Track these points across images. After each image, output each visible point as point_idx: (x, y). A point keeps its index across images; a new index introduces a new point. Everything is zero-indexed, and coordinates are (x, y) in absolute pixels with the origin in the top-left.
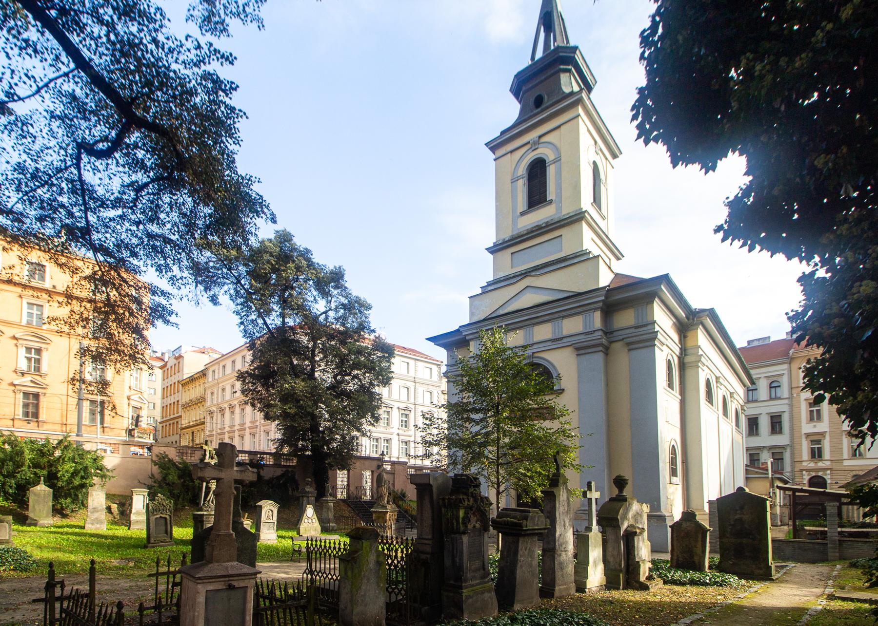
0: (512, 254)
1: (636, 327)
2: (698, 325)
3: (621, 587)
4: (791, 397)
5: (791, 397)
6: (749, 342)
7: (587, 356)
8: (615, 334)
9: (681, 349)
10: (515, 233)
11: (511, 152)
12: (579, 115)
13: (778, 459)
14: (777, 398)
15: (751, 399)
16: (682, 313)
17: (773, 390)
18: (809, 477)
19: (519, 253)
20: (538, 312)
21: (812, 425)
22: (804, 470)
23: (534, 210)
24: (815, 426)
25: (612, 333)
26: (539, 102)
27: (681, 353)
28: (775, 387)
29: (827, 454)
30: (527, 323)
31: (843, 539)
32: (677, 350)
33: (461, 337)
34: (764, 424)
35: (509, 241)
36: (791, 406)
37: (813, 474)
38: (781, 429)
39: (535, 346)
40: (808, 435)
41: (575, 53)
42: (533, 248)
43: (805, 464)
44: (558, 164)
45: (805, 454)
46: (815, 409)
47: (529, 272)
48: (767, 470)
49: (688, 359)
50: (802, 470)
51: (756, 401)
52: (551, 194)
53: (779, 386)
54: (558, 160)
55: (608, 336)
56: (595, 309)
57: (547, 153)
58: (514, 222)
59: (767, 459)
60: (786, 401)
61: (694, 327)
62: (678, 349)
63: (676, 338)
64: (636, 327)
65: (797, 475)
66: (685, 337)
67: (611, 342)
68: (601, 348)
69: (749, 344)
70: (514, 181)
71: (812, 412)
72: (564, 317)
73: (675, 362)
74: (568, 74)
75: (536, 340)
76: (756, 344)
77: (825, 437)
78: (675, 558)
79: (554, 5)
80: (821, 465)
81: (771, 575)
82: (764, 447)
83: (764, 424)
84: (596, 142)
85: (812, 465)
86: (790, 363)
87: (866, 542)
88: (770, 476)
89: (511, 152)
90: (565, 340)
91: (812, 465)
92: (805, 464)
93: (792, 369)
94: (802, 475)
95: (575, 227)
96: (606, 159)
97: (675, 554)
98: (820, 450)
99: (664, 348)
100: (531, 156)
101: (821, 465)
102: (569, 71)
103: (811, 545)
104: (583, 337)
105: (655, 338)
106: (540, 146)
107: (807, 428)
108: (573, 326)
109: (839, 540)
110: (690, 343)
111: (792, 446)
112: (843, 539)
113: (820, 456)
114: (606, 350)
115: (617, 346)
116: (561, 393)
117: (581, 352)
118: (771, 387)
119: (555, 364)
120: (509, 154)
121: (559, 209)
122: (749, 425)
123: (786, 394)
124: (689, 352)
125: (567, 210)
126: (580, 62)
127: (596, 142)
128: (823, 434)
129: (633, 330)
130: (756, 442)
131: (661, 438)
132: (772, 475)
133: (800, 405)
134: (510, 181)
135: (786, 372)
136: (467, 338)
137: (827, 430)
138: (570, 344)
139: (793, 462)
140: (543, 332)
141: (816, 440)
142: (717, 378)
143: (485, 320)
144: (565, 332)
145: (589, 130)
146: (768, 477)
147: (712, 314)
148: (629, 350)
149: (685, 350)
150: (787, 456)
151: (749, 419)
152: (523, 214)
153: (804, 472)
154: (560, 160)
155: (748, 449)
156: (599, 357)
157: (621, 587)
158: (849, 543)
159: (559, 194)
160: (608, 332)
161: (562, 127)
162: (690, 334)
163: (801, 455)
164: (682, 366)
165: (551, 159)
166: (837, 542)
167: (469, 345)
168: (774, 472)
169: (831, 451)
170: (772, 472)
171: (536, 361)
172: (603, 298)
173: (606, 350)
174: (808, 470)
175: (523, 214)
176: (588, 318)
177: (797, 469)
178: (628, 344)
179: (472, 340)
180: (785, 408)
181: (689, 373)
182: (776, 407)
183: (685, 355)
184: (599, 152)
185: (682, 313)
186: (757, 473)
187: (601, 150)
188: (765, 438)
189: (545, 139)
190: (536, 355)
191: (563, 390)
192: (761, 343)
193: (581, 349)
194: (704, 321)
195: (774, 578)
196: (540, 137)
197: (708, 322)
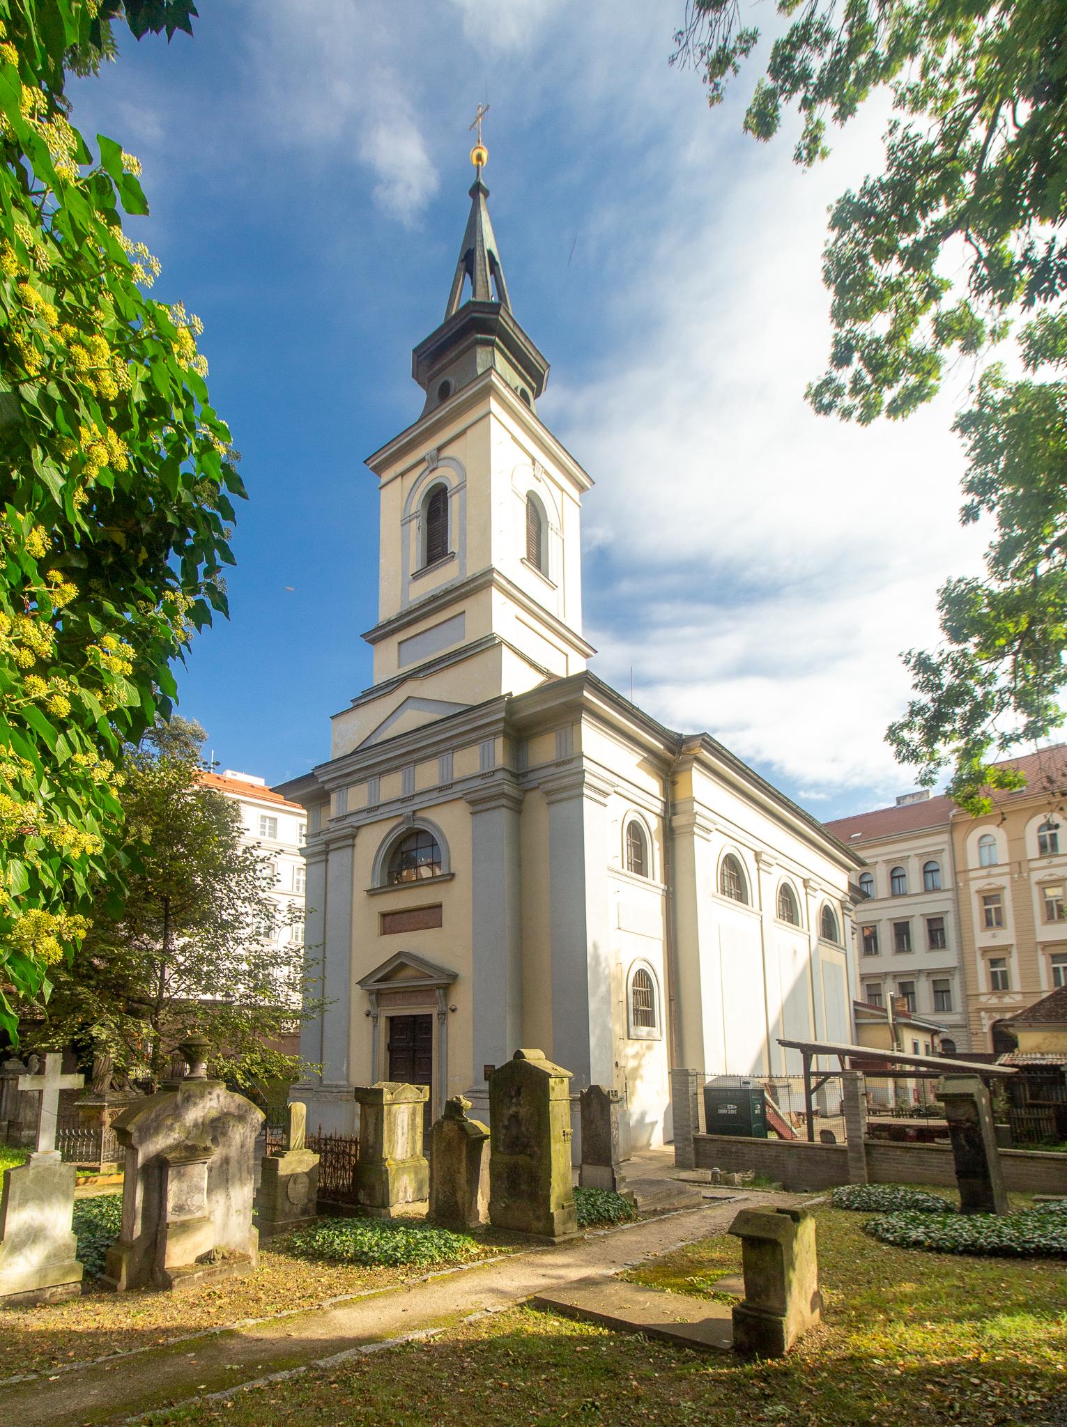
0: (400, 643)
1: (558, 765)
2: (690, 761)
3: (124, 1282)
4: (956, 889)
5: (956, 889)
6: (899, 800)
7: (485, 815)
8: (531, 776)
9: (665, 804)
10: (407, 607)
11: (402, 474)
12: (490, 412)
13: (942, 992)
14: (936, 889)
15: (930, 886)
16: (658, 745)
17: (929, 875)
18: (991, 1022)
19: (410, 641)
20: (417, 741)
21: (989, 933)
22: (983, 1009)
23: (436, 568)
24: (994, 936)
25: (525, 775)
26: (445, 393)
27: (666, 811)
28: (932, 871)
29: (1016, 983)
30: (396, 763)
31: (876, 1141)
32: (658, 807)
33: (315, 787)
34: (919, 933)
35: (397, 620)
36: (957, 902)
37: (998, 1017)
38: (943, 942)
39: (417, 800)
40: (985, 951)
41: (498, 313)
42: (427, 634)
43: (983, 999)
44: (462, 492)
45: (983, 984)
46: (992, 907)
47: (420, 671)
48: (886, 1011)
49: (678, 821)
50: (979, 1010)
51: (905, 895)
52: (453, 546)
53: (938, 870)
54: (462, 487)
55: (522, 780)
56: (495, 735)
57: (446, 474)
58: (405, 592)
59: (890, 991)
60: (949, 895)
61: (687, 766)
62: (659, 804)
63: (654, 786)
64: (558, 765)
65: (973, 1017)
66: (674, 783)
67: (527, 791)
68: (504, 802)
69: (899, 803)
70: (405, 522)
71: (988, 911)
72: (455, 749)
73: (653, 824)
74: (490, 349)
75: (418, 788)
76: (909, 801)
77: (1010, 953)
78: (434, 1196)
79: (479, 238)
80: (1007, 1000)
81: (552, 1233)
82: (886, 974)
83: (886, 937)
84: (534, 460)
85: (994, 1001)
86: (951, 833)
87: (907, 1149)
88: (891, 1021)
89: (402, 474)
90: (456, 788)
91: (994, 1001)
92: (983, 999)
93: (955, 842)
94: (980, 1019)
95: (481, 596)
96: (562, 490)
97: (435, 1187)
98: (1004, 974)
99: (613, 800)
100: (429, 481)
101: (1007, 1000)
102: (491, 343)
103: (824, 1153)
104: (478, 782)
105: (581, 783)
106: (441, 463)
107: (984, 939)
108: (467, 762)
109: (866, 1145)
110: (681, 794)
111: (962, 968)
112: (876, 1141)
113: (1006, 986)
114: (518, 807)
115: (535, 798)
116: (451, 880)
117: (479, 808)
118: (925, 872)
119: (439, 824)
120: (399, 479)
121: (463, 567)
122: (896, 935)
123: (948, 883)
124: (680, 808)
125: (472, 570)
126: (510, 327)
127: (534, 460)
128: (1006, 948)
129: (553, 770)
130: (877, 965)
131: (597, 958)
132: (894, 1020)
133: (969, 897)
134: (399, 523)
135: (946, 846)
136: (327, 787)
137: (1013, 941)
138: (459, 795)
139: (966, 997)
140: (428, 775)
141: (996, 960)
142: (757, 855)
143: (354, 753)
144: (457, 775)
145: (514, 438)
146: (887, 1024)
147: (707, 741)
148: (549, 804)
149: (674, 806)
150: (955, 986)
151: (895, 924)
152: (417, 576)
153: (983, 1014)
154: (465, 486)
155: (863, 978)
156: (501, 819)
157: (124, 1282)
158: (882, 1150)
159: (463, 544)
160: (520, 774)
161: (469, 432)
162: (681, 779)
163: (977, 985)
164: (669, 834)
165: (453, 486)
166: (863, 1149)
167: (329, 802)
168: (896, 1013)
169: (1024, 977)
170: (893, 1013)
171: (419, 825)
172: (503, 715)
173: (518, 807)
174: (989, 1010)
175: (417, 576)
176: (486, 748)
177: (971, 1009)
178: (548, 793)
179: (333, 790)
180: (949, 906)
181: (681, 843)
182: (937, 904)
183: (674, 814)
184: (544, 476)
185: (658, 745)
186: (873, 1016)
187: (546, 473)
188: (888, 960)
189: (447, 452)
190: (419, 815)
191: (453, 875)
192: (916, 801)
193: (478, 804)
194: (699, 755)
195: (556, 1240)
196: (440, 449)
197: (706, 755)
